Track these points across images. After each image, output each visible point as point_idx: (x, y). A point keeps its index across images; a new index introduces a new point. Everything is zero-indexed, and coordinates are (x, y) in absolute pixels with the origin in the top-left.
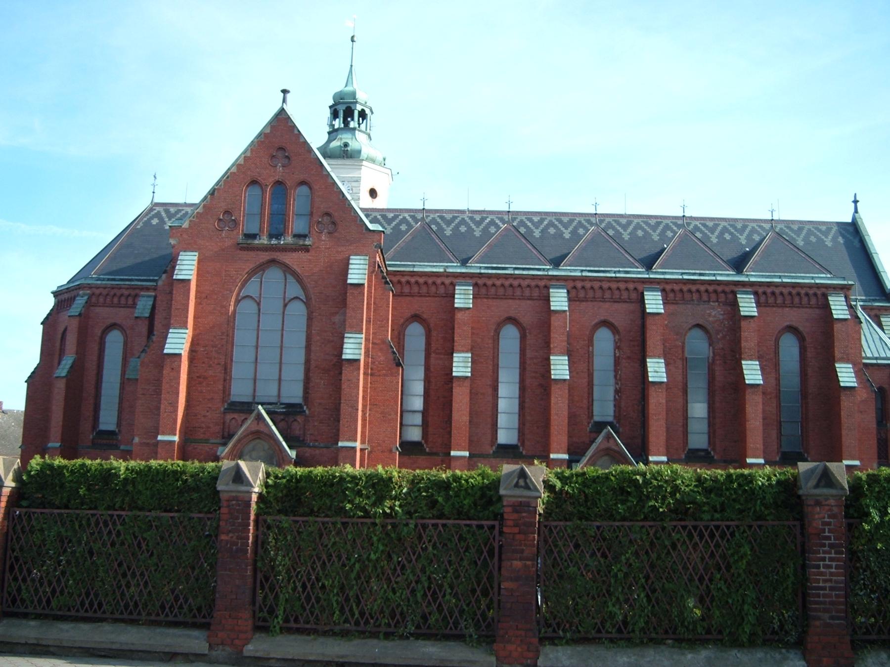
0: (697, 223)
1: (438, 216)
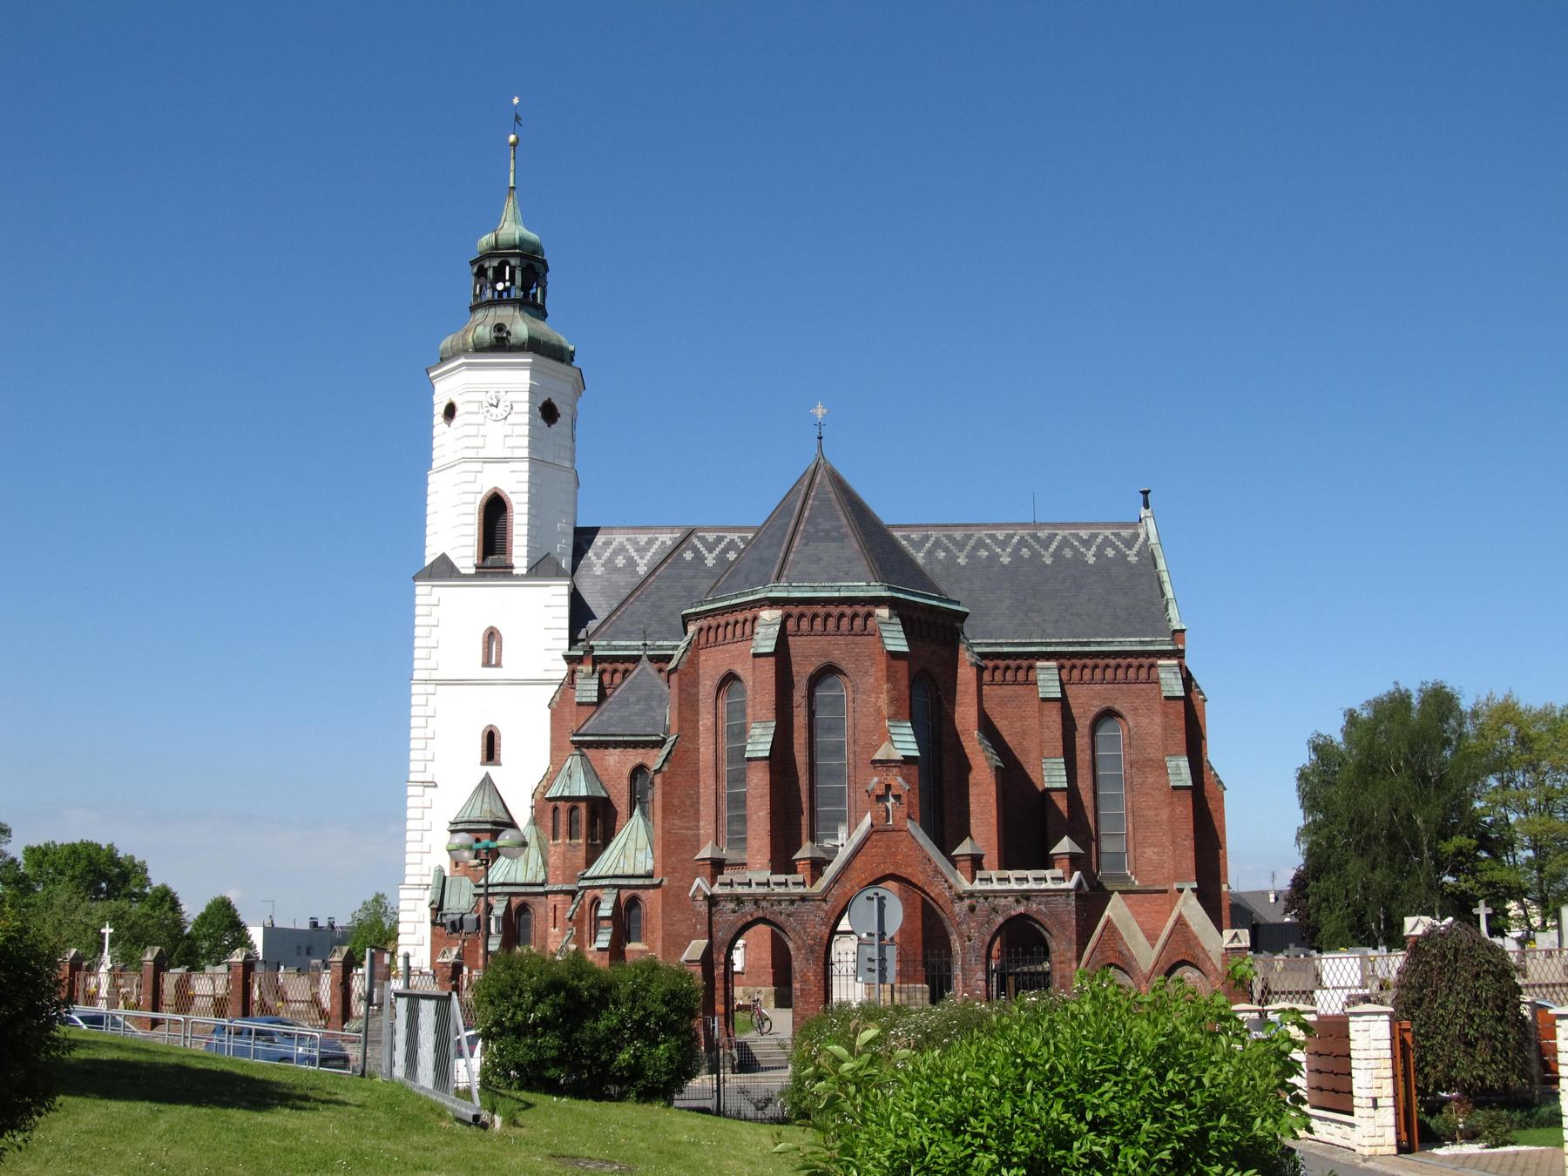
0: (1108, 532)
1: (1028, 534)
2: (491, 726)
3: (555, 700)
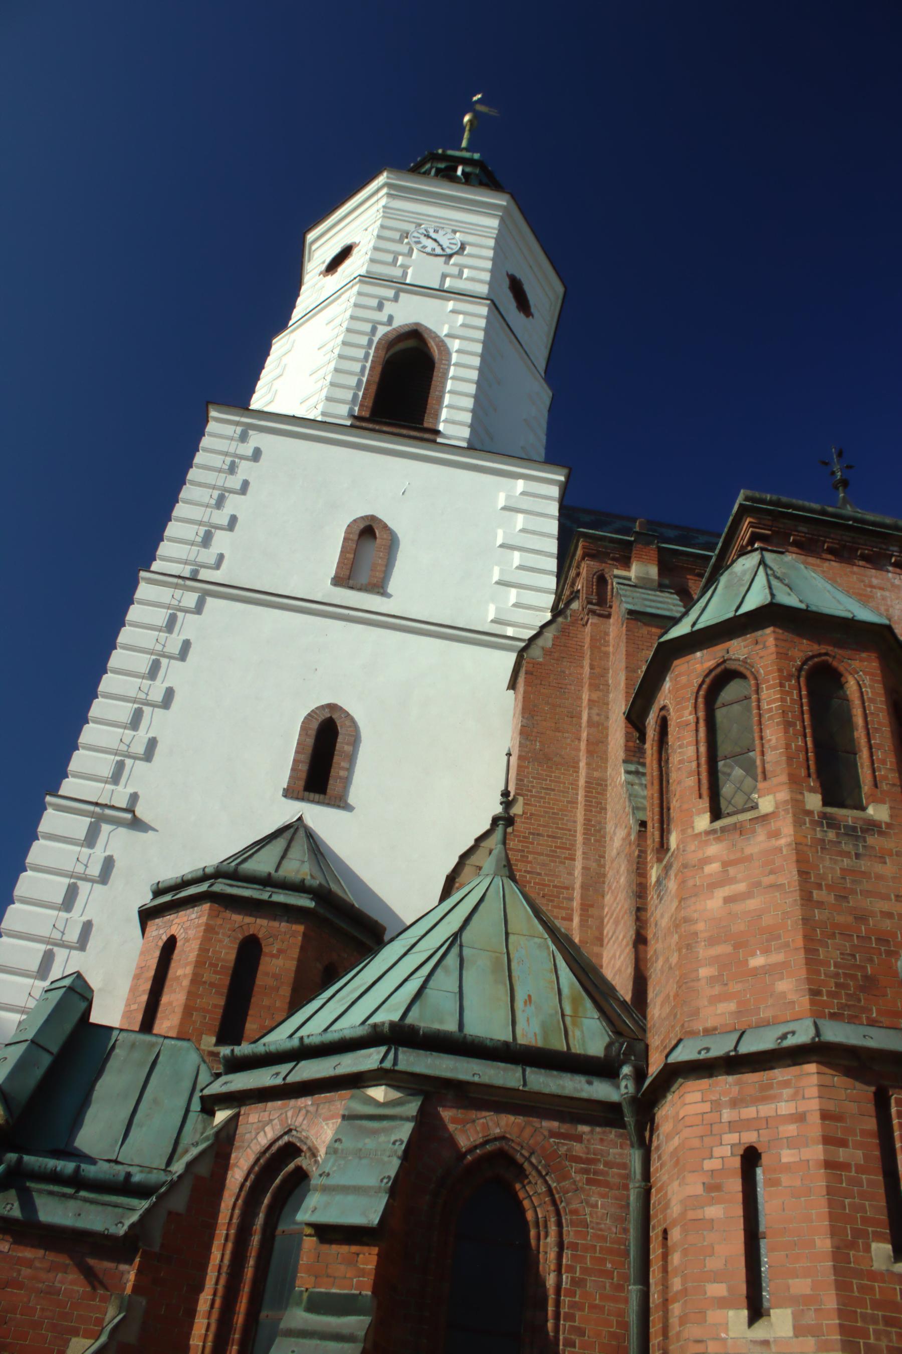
2: (333, 707)
3: (540, 642)
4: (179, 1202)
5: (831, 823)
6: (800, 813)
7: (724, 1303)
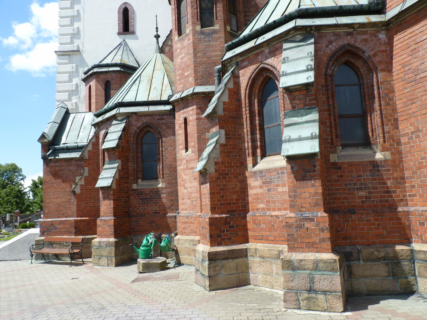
2: (125, 3)
4: (90, 148)
5: (202, 33)
6: (195, 32)
7: (182, 149)
